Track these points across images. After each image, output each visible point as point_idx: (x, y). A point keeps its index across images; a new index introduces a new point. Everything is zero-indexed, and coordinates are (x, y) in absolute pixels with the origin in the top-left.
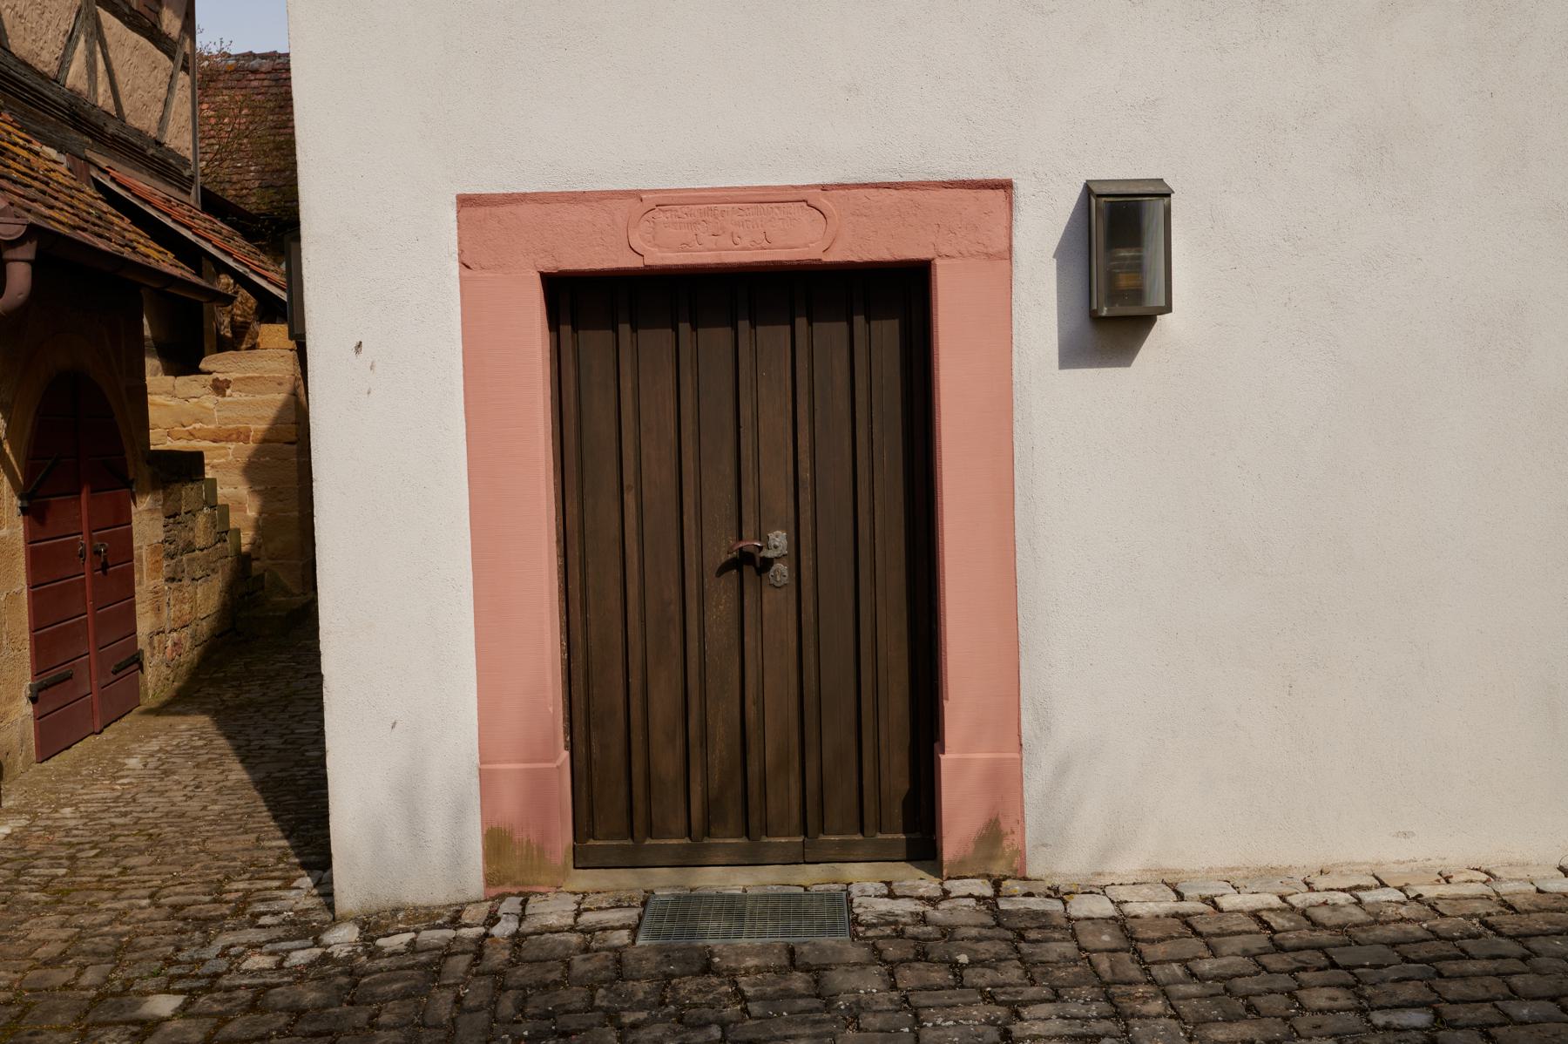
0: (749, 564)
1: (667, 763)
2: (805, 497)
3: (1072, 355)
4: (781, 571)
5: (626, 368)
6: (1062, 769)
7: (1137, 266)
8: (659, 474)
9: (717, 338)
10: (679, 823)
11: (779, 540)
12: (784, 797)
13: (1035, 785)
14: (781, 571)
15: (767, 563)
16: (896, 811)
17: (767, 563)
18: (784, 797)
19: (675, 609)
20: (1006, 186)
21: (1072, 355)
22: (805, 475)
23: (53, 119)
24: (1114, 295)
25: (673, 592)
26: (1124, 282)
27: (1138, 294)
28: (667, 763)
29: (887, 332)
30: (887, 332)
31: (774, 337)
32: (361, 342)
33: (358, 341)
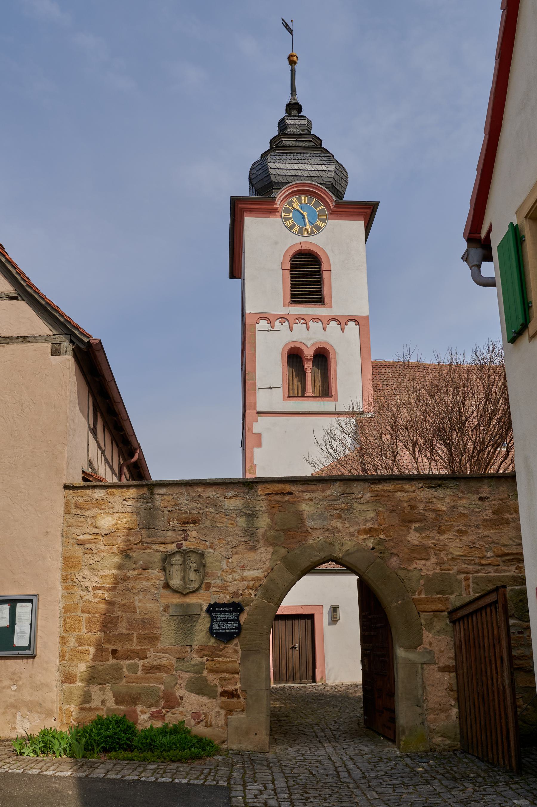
0: (294, 648)
1: (284, 671)
2: (300, 640)
3: (329, 624)
4: (297, 649)
5: (280, 627)
6: (329, 671)
7: (336, 615)
8: (284, 637)
9: (290, 622)
10: (285, 679)
11: (297, 645)
12: (298, 675)
13: (326, 672)
14: (297, 649)
15: (296, 648)
16: (311, 677)
17: (296, 648)
18: (298, 675)
19: (285, 653)
20: (322, 606)
21: (329, 624)
22: (300, 637)
23: (486, 455)
24: (334, 618)
25: (285, 651)
26: (335, 616)
27: (336, 618)
28: (284, 671)
29: (309, 621)
30: (309, 621)
31: (297, 622)
32: (343, 332)
33: (345, 331)
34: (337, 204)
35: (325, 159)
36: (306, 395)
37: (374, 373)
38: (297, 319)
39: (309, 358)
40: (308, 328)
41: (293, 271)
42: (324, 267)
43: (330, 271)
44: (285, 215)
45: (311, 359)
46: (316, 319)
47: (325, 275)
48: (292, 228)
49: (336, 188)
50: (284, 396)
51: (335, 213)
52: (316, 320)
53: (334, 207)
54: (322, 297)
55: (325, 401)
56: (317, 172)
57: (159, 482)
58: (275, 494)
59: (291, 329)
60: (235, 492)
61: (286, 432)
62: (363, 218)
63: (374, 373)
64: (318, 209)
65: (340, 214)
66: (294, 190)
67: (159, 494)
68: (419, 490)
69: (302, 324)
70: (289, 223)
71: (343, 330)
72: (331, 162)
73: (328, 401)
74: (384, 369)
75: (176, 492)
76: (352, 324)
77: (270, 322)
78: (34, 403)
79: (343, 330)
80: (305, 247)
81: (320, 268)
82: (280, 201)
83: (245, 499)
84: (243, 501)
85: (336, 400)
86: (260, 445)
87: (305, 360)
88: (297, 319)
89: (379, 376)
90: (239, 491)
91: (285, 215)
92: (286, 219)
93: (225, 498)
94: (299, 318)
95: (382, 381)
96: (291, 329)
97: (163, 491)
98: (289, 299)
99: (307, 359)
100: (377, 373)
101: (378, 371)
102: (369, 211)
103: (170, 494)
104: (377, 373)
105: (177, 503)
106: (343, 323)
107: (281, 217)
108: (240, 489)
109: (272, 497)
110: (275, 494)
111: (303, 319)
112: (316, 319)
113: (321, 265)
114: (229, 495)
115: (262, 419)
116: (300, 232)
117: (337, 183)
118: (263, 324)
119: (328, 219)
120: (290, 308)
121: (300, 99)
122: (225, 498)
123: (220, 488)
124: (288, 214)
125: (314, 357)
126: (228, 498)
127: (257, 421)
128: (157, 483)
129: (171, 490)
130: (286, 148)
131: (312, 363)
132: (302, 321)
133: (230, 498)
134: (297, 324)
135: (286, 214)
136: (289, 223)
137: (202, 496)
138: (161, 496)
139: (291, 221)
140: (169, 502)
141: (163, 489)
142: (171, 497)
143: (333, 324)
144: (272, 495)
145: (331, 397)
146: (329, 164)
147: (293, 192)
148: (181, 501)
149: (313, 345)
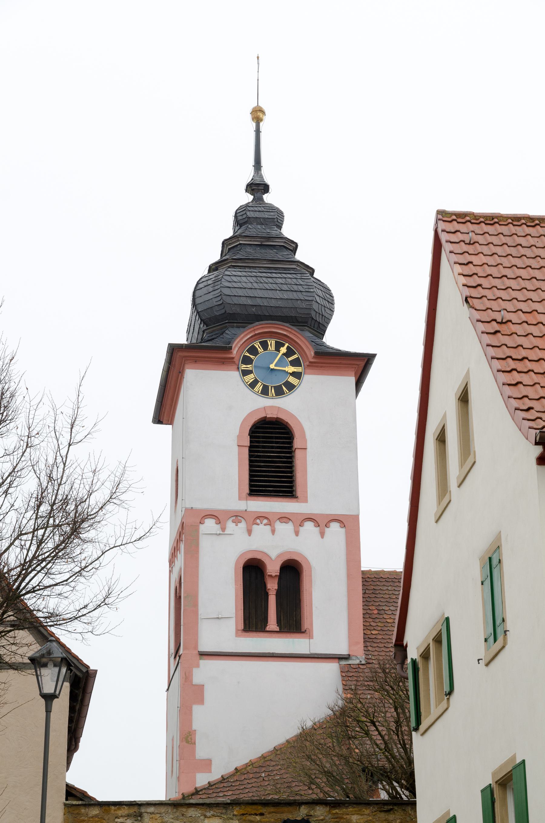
33: (325, 537)
34: (318, 354)
35: (302, 283)
36: (268, 628)
37: (367, 592)
38: (258, 518)
39: (274, 574)
40: (273, 531)
41: (252, 449)
42: (297, 443)
43: (306, 449)
44: (243, 367)
45: (276, 576)
46: (285, 518)
47: (298, 455)
48: (253, 385)
49: (316, 321)
50: (237, 630)
51: (314, 365)
52: (285, 520)
53: (314, 357)
54: (293, 486)
55: (296, 638)
56: (290, 301)
57: (148, 802)
58: (249, 814)
59: (250, 532)
60: (214, 811)
61: (239, 683)
62: (353, 373)
63: (367, 592)
64: (290, 359)
65: (321, 367)
66: (257, 332)
67: (148, 813)
68: (373, 813)
69: (265, 525)
70: (250, 378)
71: (322, 534)
72: (310, 287)
73: (299, 638)
74: (383, 584)
75: (162, 811)
76: (335, 526)
77: (219, 522)
78: (37, 727)
79: (322, 534)
80: (271, 415)
81: (291, 447)
82: (237, 349)
83: (223, 818)
84: (221, 820)
85: (310, 637)
86: (201, 701)
87: (267, 577)
88: (258, 518)
89: (374, 595)
90: (217, 811)
91: (243, 367)
92: (245, 373)
93: (206, 817)
94: (261, 517)
95: (377, 604)
96: (250, 532)
97: (152, 809)
98: (247, 490)
99: (271, 576)
100: (371, 592)
101: (372, 587)
102: (362, 364)
103: (157, 813)
104: (371, 592)
105: (163, 821)
106: (322, 524)
107: (238, 368)
108: (218, 809)
109: (247, 817)
110: (249, 814)
111: (266, 518)
112: (285, 518)
113: (293, 439)
114: (208, 814)
115: (206, 664)
116: (265, 392)
117: (321, 299)
118: (210, 525)
119: (304, 374)
120: (249, 502)
121: (268, 176)
122: (205, 817)
123: (201, 808)
124: (248, 366)
125: (280, 573)
126: (208, 818)
127: (198, 666)
128: (147, 803)
129: (159, 809)
130: (247, 261)
131: (277, 582)
132: (265, 521)
133: (210, 817)
134: (258, 525)
135: (245, 366)
136: (250, 378)
137: (185, 815)
138: (149, 814)
139: (252, 376)
140: (156, 820)
141: (151, 808)
142: (159, 815)
143: (309, 525)
144: (247, 815)
145: (303, 632)
146: (307, 290)
147: (255, 335)
148: (167, 819)
149: (279, 556)
